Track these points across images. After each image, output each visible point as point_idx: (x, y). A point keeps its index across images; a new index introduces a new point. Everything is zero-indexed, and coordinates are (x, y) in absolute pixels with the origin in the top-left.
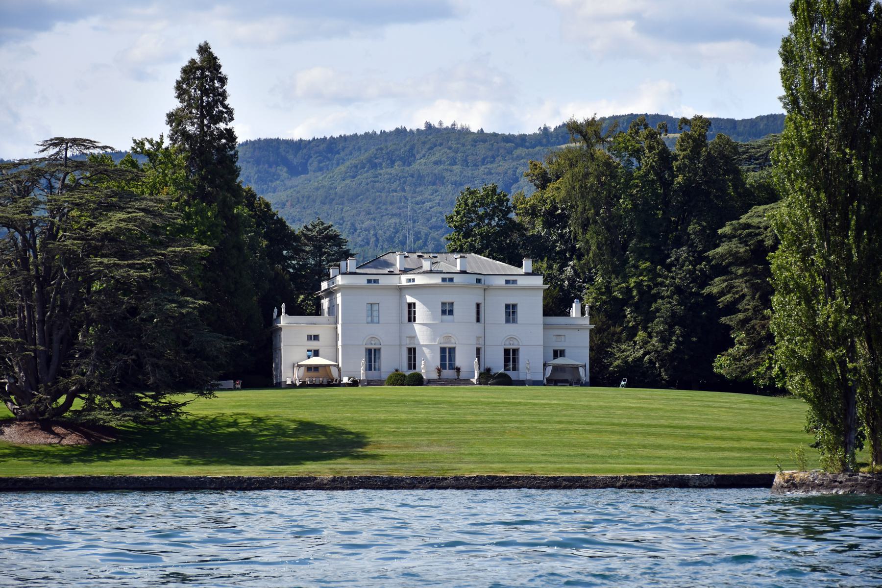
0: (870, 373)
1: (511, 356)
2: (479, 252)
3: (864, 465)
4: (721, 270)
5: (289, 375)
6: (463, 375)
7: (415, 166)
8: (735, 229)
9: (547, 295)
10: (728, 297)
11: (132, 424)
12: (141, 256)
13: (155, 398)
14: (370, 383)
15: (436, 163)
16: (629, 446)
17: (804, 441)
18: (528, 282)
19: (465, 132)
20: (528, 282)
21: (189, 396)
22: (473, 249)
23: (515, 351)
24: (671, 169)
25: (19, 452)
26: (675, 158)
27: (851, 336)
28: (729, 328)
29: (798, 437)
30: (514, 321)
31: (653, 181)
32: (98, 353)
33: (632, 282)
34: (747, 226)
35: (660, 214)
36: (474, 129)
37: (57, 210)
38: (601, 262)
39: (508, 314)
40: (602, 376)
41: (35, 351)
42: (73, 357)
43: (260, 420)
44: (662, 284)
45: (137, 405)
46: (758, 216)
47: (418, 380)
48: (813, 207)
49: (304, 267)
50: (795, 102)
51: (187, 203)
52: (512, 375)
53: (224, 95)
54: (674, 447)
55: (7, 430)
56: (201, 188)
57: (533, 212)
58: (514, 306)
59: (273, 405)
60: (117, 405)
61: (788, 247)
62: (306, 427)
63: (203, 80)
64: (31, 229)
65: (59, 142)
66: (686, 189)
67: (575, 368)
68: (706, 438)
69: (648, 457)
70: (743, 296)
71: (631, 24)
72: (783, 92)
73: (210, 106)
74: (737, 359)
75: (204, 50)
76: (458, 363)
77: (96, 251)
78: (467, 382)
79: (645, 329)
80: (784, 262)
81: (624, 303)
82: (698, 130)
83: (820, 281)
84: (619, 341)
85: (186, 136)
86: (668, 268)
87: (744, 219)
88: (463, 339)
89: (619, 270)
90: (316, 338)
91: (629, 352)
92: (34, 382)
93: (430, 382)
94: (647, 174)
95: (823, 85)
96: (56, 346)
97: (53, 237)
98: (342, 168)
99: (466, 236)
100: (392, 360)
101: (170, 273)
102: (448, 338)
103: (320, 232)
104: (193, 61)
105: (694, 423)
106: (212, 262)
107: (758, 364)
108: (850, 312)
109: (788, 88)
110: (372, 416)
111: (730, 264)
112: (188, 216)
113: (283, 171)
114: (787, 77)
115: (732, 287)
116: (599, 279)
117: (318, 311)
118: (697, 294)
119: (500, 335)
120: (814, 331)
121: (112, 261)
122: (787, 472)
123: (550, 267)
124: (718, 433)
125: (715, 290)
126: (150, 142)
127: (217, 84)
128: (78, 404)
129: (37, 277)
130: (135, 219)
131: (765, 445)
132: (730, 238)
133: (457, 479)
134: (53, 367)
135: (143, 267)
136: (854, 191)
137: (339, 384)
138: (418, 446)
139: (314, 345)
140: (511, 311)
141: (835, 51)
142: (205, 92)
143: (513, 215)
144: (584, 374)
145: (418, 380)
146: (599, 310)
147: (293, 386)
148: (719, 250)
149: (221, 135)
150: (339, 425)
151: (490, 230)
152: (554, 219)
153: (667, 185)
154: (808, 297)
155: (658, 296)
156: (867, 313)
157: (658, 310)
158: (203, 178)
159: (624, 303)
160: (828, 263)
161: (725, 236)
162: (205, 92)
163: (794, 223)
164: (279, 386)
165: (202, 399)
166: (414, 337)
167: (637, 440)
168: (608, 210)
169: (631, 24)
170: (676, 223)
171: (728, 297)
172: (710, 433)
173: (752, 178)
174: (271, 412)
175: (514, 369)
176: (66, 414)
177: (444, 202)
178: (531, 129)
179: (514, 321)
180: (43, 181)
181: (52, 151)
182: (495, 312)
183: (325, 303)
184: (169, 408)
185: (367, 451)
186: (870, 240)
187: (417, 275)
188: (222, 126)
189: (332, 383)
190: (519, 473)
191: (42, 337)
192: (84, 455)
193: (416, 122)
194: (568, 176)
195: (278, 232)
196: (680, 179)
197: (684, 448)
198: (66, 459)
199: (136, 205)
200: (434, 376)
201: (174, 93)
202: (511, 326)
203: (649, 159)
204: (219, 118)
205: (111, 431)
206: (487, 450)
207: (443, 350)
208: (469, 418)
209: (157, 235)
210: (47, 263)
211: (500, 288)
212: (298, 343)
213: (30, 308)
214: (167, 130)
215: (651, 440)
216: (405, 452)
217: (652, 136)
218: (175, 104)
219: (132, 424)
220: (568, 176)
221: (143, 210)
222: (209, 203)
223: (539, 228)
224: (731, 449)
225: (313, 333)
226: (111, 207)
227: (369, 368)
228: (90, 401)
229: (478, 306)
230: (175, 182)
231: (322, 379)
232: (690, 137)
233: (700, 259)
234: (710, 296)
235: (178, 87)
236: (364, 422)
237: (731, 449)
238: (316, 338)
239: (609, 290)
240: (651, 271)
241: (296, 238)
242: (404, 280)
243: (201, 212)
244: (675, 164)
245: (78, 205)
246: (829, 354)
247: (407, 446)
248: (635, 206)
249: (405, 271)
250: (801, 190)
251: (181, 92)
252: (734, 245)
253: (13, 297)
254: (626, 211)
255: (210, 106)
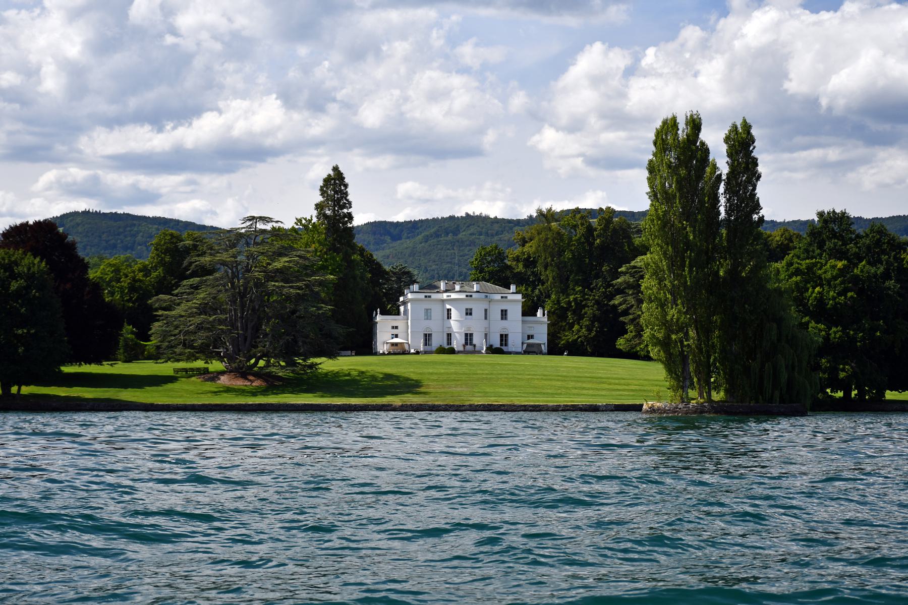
0: (697, 347)
1: (504, 338)
2: (488, 281)
3: (693, 399)
4: (620, 291)
5: (382, 348)
6: (477, 349)
7: (460, 236)
8: (628, 269)
9: (524, 305)
10: (624, 306)
11: (291, 375)
12: (297, 282)
13: (304, 360)
14: (426, 353)
15: (471, 234)
16: (567, 388)
17: (663, 386)
18: (514, 298)
19: (487, 218)
20: (514, 298)
21: (324, 359)
22: (484, 279)
23: (506, 336)
24: (593, 235)
25: (228, 390)
26: (595, 230)
27: (686, 326)
28: (624, 323)
29: (661, 383)
30: (506, 319)
31: (583, 243)
32: (273, 336)
33: (572, 298)
34: (635, 267)
35: (587, 260)
36: (492, 216)
37: (250, 256)
38: (555, 287)
39: (502, 315)
40: (554, 349)
41: (238, 334)
42: (259, 337)
43: (363, 372)
44: (588, 299)
45: (295, 364)
46: (639, 261)
47: (452, 351)
48: (665, 254)
49: (391, 289)
50: (655, 195)
51: (326, 253)
52: (504, 348)
53: (346, 194)
54: (592, 389)
55: (222, 378)
56: (334, 245)
57: (517, 259)
58: (506, 311)
59: (370, 364)
60: (283, 364)
61: (651, 277)
62: (388, 376)
63: (335, 186)
64: (236, 267)
65: (252, 218)
66: (602, 247)
67: (539, 345)
68: (610, 384)
69: (578, 394)
70: (632, 306)
71: (581, 159)
72: (649, 190)
73: (339, 200)
74: (628, 340)
75: (336, 169)
76: (474, 342)
77: (272, 279)
78: (480, 352)
79: (578, 324)
80: (648, 284)
81: (567, 309)
82: (607, 215)
83: (669, 296)
84: (564, 330)
85: (326, 216)
86: (591, 290)
87: (633, 263)
88: (477, 327)
89: (565, 291)
90: (397, 328)
91: (568, 337)
92: (237, 351)
93: (459, 352)
94: (580, 239)
95: (671, 186)
96: (249, 331)
97: (248, 270)
98: (420, 237)
99: (480, 273)
100: (438, 341)
101: (312, 291)
102: (469, 328)
103: (400, 270)
104: (329, 175)
105: (603, 376)
106: (339, 287)
107: (640, 344)
108: (686, 313)
109: (651, 187)
110: (426, 371)
111: (625, 288)
112: (326, 260)
113: (388, 239)
114: (651, 181)
115: (626, 301)
116: (553, 297)
117: (398, 314)
118: (607, 305)
119: (498, 327)
120: (666, 325)
121: (280, 284)
122: (650, 403)
123: (527, 290)
124: (617, 381)
125: (616, 302)
126: (305, 219)
127: (343, 188)
128: (262, 363)
129: (239, 293)
130: (294, 261)
131: (642, 388)
132: (624, 273)
133: (470, 405)
134: (248, 343)
135: (299, 288)
136: (688, 245)
137: (409, 353)
138: (450, 387)
139: (395, 332)
140: (504, 314)
141: (677, 167)
142: (336, 192)
143: (506, 261)
144: (544, 348)
145: (452, 351)
146: (554, 313)
147: (384, 354)
148: (619, 280)
149: (345, 215)
150: (406, 375)
151: (496, 272)
152: (529, 262)
153: (591, 244)
154: (662, 305)
155: (586, 306)
156: (695, 313)
157: (586, 313)
158: (335, 240)
159: (567, 309)
160: (673, 286)
161: (622, 272)
162: (336, 192)
163: (654, 263)
164: (376, 354)
165: (330, 361)
166: (450, 327)
167: (572, 384)
168: (558, 258)
169: (581, 159)
170: (596, 266)
171: (624, 306)
172: (613, 381)
173: (637, 241)
174: (369, 368)
175: (506, 345)
176: (256, 369)
177: (473, 255)
178: (524, 216)
179: (506, 319)
180: (243, 241)
181: (248, 223)
182: (496, 314)
183: (402, 308)
184: (312, 366)
185: (422, 390)
186: (697, 273)
187: (453, 296)
188: (345, 211)
189: (405, 353)
190: (505, 402)
191: (242, 327)
192: (264, 392)
193: (460, 213)
194: (537, 239)
195: (376, 269)
196: (598, 241)
197: (598, 390)
198: (254, 394)
199: (295, 253)
200: (461, 349)
201: (319, 193)
202: (504, 321)
203: (581, 230)
204: (344, 207)
205: (280, 378)
206: (488, 390)
207: (466, 335)
208: (479, 372)
209: (308, 269)
210: (245, 286)
211: (498, 301)
212: (387, 331)
213: (235, 309)
214: (315, 213)
215: (579, 385)
216: (443, 390)
217: (582, 218)
218: (320, 199)
219: (291, 375)
220: (537, 239)
221: (298, 256)
222: (338, 254)
223: (520, 268)
224: (624, 390)
225: (395, 325)
226: (281, 255)
227: (425, 344)
228: (268, 362)
229: (486, 310)
230: (319, 242)
231: (399, 351)
232: (604, 218)
233: (609, 285)
234: (614, 305)
235: (321, 189)
236: (421, 374)
237: (624, 390)
238: (397, 328)
239: (559, 302)
240: (582, 292)
241: (387, 273)
242: (445, 296)
243: (333, 258)
244: (595, 233)
245: (262, 253)
246: (674, 337)
247: (444, 387)
248: (574, 255)
249: (446, 291)
250: (658, 244)
251: (323, 192)
252: (627, 278)
253: (227, 304)
254: (569, 259)
255: (339, 200)
